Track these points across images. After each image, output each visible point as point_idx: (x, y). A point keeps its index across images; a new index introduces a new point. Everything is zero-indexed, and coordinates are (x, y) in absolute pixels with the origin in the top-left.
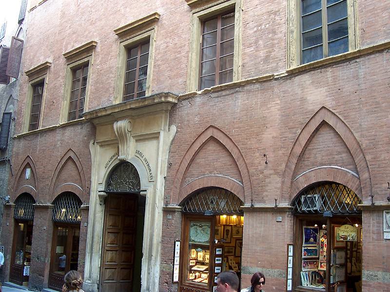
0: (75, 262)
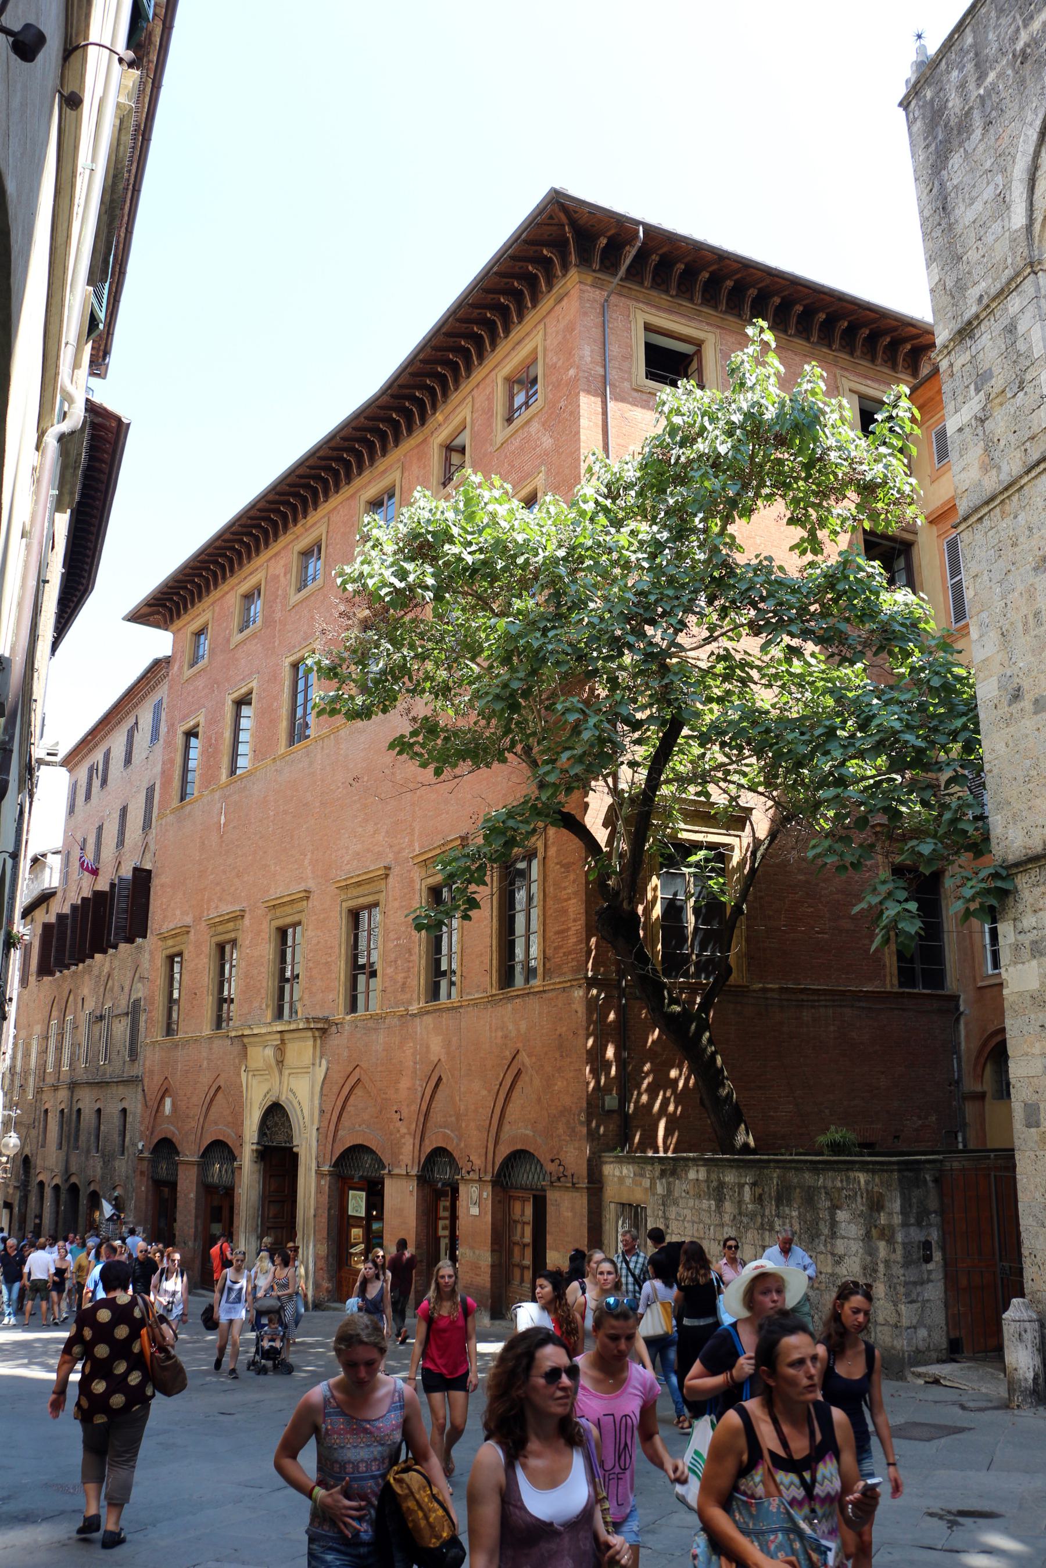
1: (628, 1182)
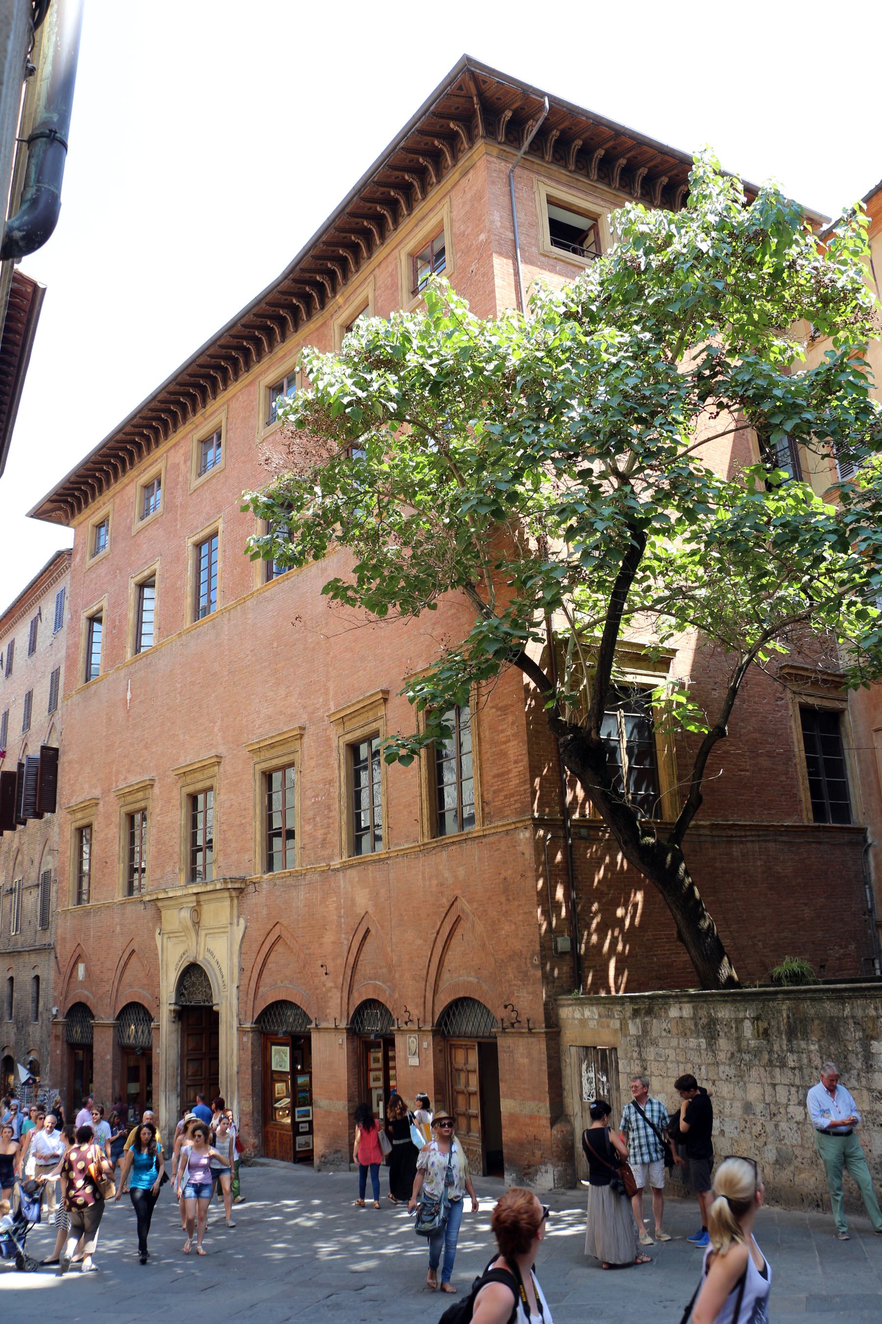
0: (407, 1140)
1: (592, 1024)
